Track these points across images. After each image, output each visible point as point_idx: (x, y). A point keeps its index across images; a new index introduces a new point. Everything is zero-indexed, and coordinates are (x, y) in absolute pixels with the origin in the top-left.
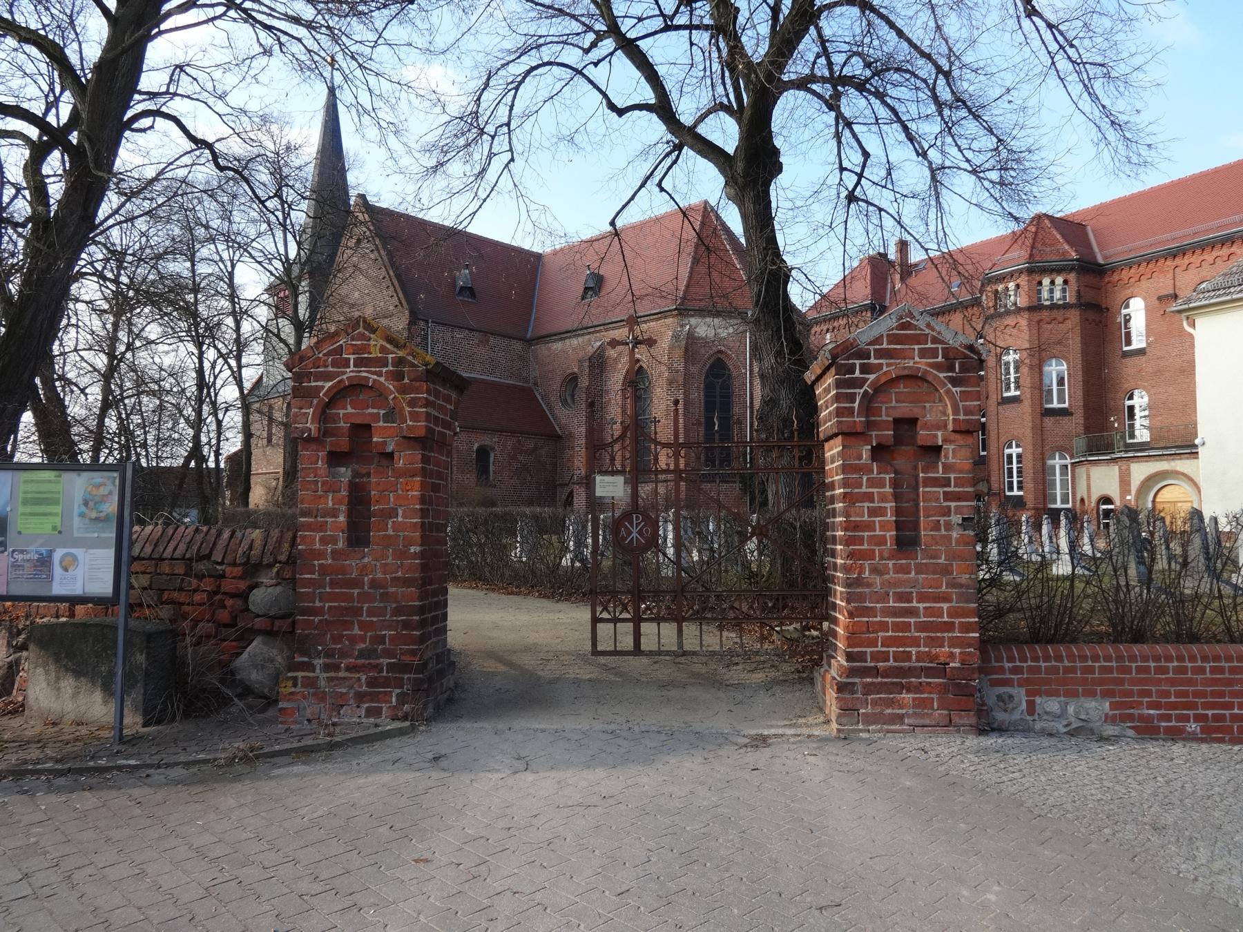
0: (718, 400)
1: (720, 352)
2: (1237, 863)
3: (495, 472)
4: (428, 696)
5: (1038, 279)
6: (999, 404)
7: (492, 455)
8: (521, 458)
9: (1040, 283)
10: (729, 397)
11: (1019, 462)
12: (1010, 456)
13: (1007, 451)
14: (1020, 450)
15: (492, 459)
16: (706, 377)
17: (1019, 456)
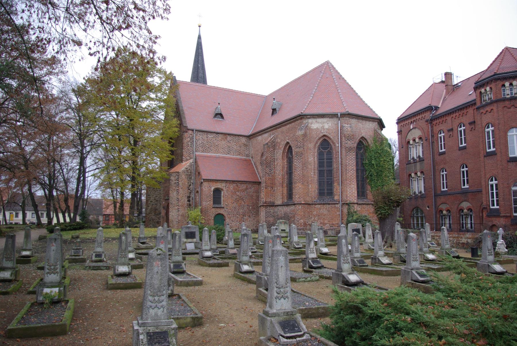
0: (325, 161)
1: (324, 136)
2: (441, 343)
3: (224, 201)
4: (38, 176)
5: (502, 83)
6: (485, 156)
7: (222, 192)
8: (238, 193)
9: (504, 85)
10: (331, 159)
11: (497, 189)
12: (492, 186)
13: (490, 183)
14: (496, 182)
15: (222, 195)
16: (319, 149)
17: (496, 185)
